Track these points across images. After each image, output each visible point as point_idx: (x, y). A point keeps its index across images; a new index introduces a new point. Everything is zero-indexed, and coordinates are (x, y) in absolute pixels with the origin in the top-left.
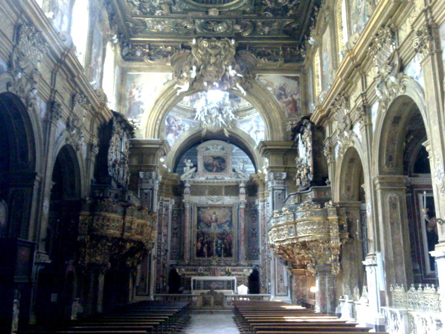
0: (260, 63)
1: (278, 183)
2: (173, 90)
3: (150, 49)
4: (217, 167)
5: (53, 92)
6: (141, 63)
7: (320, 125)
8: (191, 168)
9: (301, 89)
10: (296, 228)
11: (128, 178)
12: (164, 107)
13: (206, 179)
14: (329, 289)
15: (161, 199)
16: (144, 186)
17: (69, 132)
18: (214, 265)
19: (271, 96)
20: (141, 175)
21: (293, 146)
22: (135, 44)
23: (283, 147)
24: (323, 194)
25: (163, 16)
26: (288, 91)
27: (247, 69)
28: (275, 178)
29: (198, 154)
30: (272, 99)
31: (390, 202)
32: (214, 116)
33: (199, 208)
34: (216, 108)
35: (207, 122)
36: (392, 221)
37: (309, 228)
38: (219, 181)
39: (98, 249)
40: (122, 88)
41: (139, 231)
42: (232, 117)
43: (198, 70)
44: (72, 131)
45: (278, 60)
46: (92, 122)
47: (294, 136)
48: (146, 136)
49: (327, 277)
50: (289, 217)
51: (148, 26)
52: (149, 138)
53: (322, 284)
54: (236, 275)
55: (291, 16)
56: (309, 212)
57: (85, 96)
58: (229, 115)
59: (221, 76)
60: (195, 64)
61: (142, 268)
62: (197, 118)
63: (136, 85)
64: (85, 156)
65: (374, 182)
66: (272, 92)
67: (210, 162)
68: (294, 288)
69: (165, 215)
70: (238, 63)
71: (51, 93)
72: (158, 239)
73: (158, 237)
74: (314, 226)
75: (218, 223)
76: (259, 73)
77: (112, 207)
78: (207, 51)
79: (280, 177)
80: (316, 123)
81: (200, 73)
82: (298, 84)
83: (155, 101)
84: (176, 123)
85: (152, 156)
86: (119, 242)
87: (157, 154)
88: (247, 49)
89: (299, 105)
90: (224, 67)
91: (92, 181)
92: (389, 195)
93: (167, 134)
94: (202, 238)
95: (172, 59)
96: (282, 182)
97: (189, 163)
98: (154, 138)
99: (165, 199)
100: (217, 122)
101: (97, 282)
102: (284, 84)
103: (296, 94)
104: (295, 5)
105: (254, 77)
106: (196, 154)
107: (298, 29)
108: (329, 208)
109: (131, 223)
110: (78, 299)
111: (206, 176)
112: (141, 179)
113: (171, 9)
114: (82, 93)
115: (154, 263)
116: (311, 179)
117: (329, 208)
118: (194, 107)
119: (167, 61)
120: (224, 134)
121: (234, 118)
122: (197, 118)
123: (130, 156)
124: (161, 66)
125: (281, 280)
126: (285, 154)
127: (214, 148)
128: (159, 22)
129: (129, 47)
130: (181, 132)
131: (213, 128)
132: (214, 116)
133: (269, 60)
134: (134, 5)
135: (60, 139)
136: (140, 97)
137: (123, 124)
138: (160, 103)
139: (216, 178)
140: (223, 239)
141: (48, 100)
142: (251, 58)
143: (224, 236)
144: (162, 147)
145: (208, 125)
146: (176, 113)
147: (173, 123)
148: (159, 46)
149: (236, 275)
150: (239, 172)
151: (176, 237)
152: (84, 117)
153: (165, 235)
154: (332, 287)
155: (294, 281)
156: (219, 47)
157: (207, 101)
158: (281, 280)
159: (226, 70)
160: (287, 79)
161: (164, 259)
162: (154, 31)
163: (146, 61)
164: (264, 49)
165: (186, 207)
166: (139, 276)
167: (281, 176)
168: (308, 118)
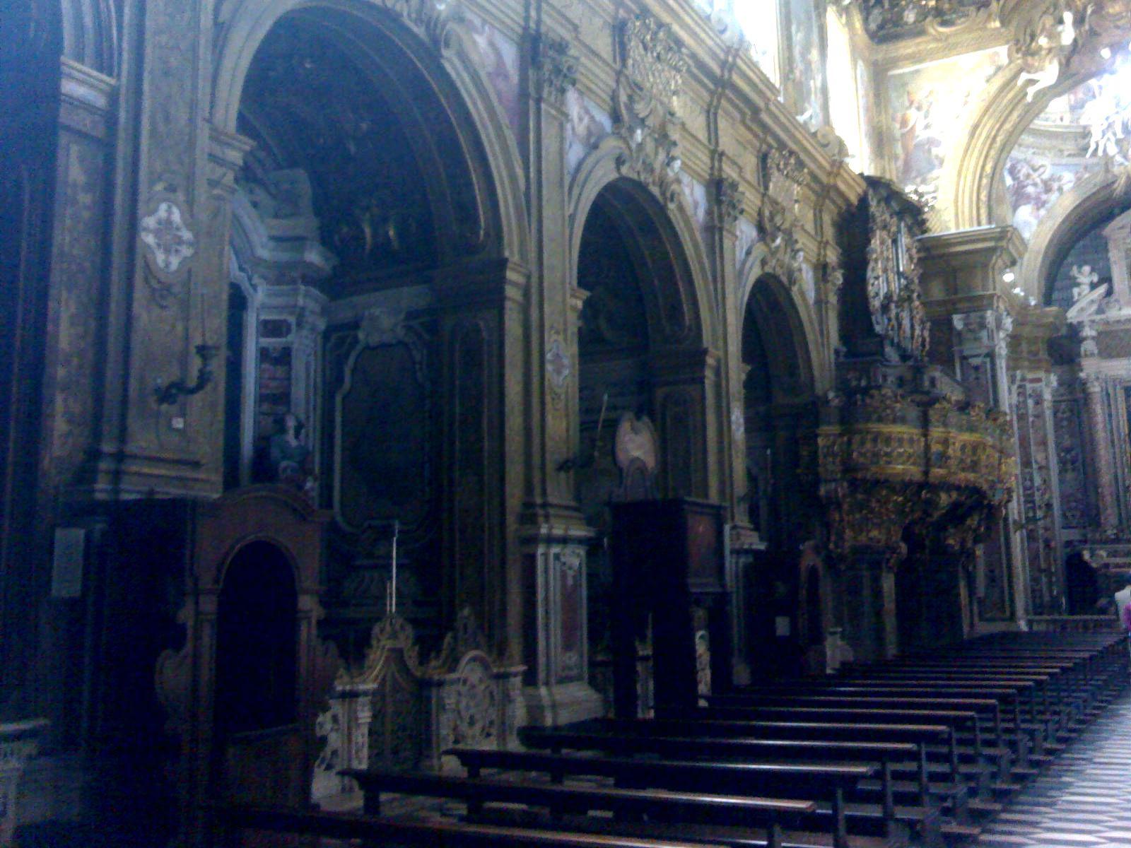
6: (919, 40)
8: (1093, 286)
17: (767, 245)
20: (958, 322)
29: (1111, 246)
39: (872, 511)
40: (880, 114)
41: (969, 461)
43: (1079, 21)
44: (774, 241)
48: (957, 226)
52: (966, 228)
62: (1096, 150)
64: (811, 296)
71: (712, 159)
83: (968, 128)
84: (1035, 175)
91: (837, 352)
93: (1015, 208)
97: (1085, 275)
98: (979, 224)
101: (878, 593)
109: (946, 442)
112: (959, 334)
114: (782, 145)
115: (1017, 538)
118: (1083, 122)
119: (989, 18)
122: (1096, 150)
123: (923, 279)
130: (1053, 197)
136: (927, 127)
138: (984, 132)
144: (1004, 243)
146: (1031, 151)
147: (1028, 176)
151: (1074, 470)
153: (1040, 468)
161: (1046, 529)
165: (1092, 390)
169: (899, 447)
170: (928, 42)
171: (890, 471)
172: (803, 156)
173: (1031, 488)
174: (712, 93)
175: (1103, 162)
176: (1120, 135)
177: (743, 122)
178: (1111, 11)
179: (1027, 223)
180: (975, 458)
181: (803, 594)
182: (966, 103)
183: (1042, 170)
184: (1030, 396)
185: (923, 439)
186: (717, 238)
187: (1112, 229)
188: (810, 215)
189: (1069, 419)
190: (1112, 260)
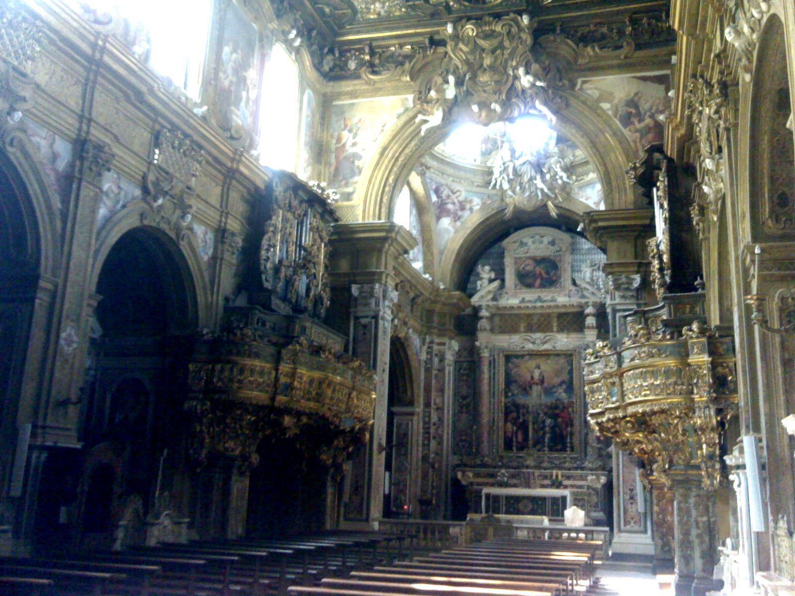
0: (583, 57)
1: (623, 297)
2: (412, 128)
3: (372, 53)
4: (542, 279)
5: (85, 121)
6: (356, 82)
8: (491, 281)
10: (622, 385)
12: (397, 159)
13: (521, 302)
15: (428, 340)
18: (527, 467)
19: (608, 122)
20: (355, 290)
22: (346, 47)
23: (632, 222)
24: (688, 310)
26: (645, 106)
27: (558, 69)
28: (617, 287)
29: (506, 254)
31: (781, 310)
32: (526, 179)
33: (508, 358)
34: (530, 163)
35: (514, 192)
36: (787, 356)
37: (645, 384)
38: (545, 304)
39: (227, 426)
40: (323, 131)
41: (314, 393)
42: (561, 178)
43: (459, 83)
45: (621, 47)
48: (364, 217)
50: (609, 361)
52: (370, 220)
54: (572, 486)
56: (645, 349)
58: (556, 174)
59: (505, 89)
62: (495, 184)
63: (349, 123)
65: (744, 261)
66: (610, 113)
67: (528, 268)
69: (439, 370)
71: (81, 122)
72: (424, 417)
73: (424, 412)
74: (656, 379)
75: (545, 385)
76: (584, 76)
77: (250, 346)
79: (627, 283)
83: (380, 150)
84: (453, 197)
85: (375, 254)
86: (269, 414)
87: (385, 250)
88: (558, 32)
90: (511, 72)
92: (781, 290)
93: (439, 218)
94: (514, 415)
95: (413, 68)
96: (631, 294)
97: (485, 272)
98: (379, 219)
100: (533, 189)
102: (636, 94)
103: (662, 112)
105: (574, 85)
106: (501, 255)
108: (692, 338)
109: (293, 375)
110: (187, 520)
111: (521, 296)
112: (356, 299)
117: (692, 338)
118: (489, 164)
120: (548, 213)
121: (565, 179)
122: (495, 184)
124: (393, 84)
125: (632, 498)
126: (636, 238)
127: (533, 244)
129: (334, 54)
130: (466, 214)
131: (525, 202)
132: (526, 179)
133: (601, 48)
136: (354, 144)
137: (300, 193)
138: (390, 154)
139: (539, 299)
140: (555, 417)
141: (74, 136)
142: (565, 48)
143: (557, 411)
145: (516, 198)
146: (451, 179)
147: (448, 197)
148: (388, 47)
149: (572, 486)
150: (584, 285)
151: (467, 413)
153: (438, 409)
156: (500, 34)
157: (513, 152)
158: (632, 498)
159: (516, 78)
162: (372, 17)
163: (364, 76)
164: (592, 27)
165: (482, 355)
167: (630, 281)
170: (361, 84)
171: (241, 395)
173: (429, 423)
174: (89, 70)
175: (499, 194)
176: (511, 177)
178: (481, 79)
179: (447, 230)
180: (319, 391)
182: (382, 130)
183: (458, 194)
184: (436, 355)
185: (274, 372)
186: (75, 186)
188: (218, 190)
189: (468, 375)
190: (506, 264)
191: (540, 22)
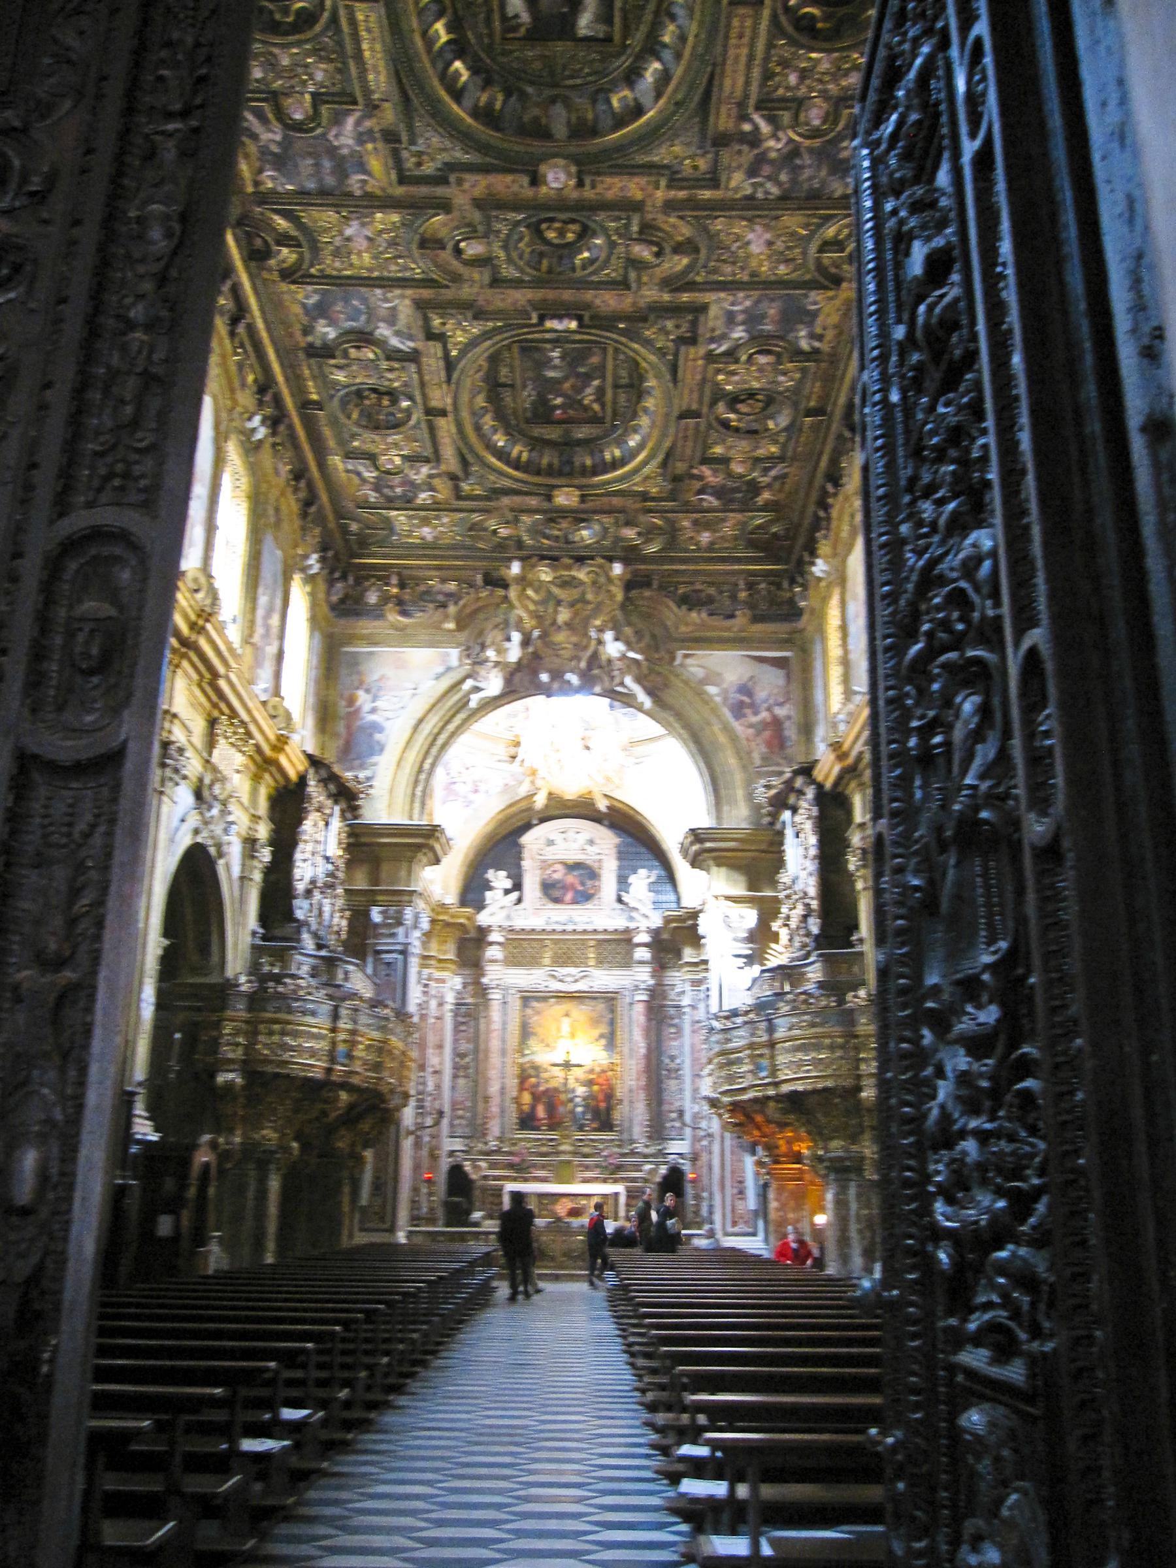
3: (402, 586)
4: (577, 892)
7: (840, 789)
8: (507, 892)
9: (796, 694)
10: (772, 1057)
11: (344, 923)
14: (858, 1215)
16: (384, 944)
17: (201, 814)
19: (714, 711)
20: (376, 915)
21: (771, 844)
25: (437, 507)
26: (761, 694)
27: (654, 636)
30: (718, 717)
43: (525, 643)
46: (256, 778)
47: (775, 816)
49: (853, 1184)
51: (398, 528)
53: (841, 1204)
55: (765, 508)
57: (242, 722)
60: (519, 628)
61: (377, 1156)
64: (236, 871)
66: (718, 699)
67: (556, 876)
68: (773, 1215)
70: (629, 624)
78: (549, 592)
80: (828, 785)
81: (531, 649)
82: (788, 677)
83: (413, 722)
89: (791, 732)
90: (593, 634)
91: (254, 933)
95: (460, 612)
97: (499, 879)
98: (411, 818)
99: (437, 974)
101: (262, 1194)
102: (752, 678)
103: (781, 704)
104: (776, 478)
105: (673, 658)
107: (786, 538)
113: (457, 488)
114: (234, 714)
115: (407, 1144)
116: (815, 930)
119: (446, 617)
123: (350, 864)
128: (425, 521)
134: (364, 481)
135: (180, 833)
136: (374, 711)
138: (428, 728)
144: (431, 842)
152: (238, 772)
154: (866, 1212)
155: (771, 1195)
156: (582, 583)
159: (600, 642)
160: (757, 664)
161: (433, 1137)
166: (368, 1177)
168: (807, 771)
169: (308, 1043)
172: (253, 728)
174: (202, 630)
177: (200, 686)
181: (192, 1192)
187: (527, 839)
191: (635, 573)
